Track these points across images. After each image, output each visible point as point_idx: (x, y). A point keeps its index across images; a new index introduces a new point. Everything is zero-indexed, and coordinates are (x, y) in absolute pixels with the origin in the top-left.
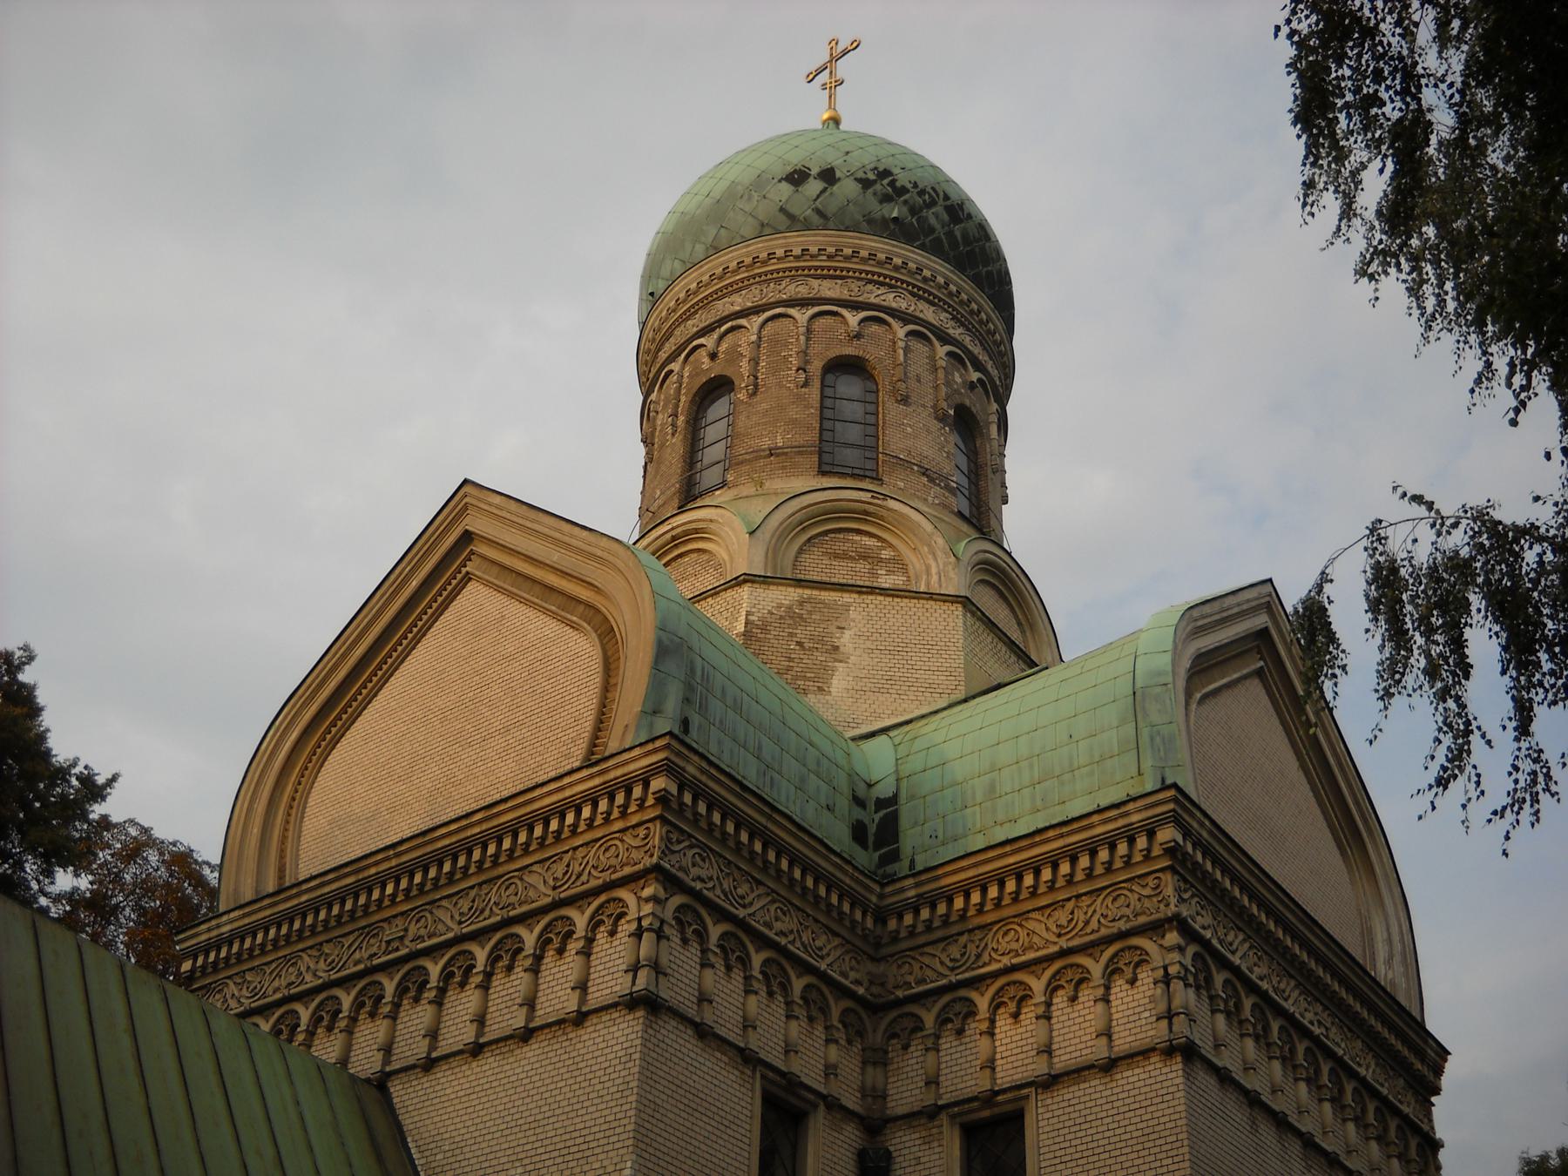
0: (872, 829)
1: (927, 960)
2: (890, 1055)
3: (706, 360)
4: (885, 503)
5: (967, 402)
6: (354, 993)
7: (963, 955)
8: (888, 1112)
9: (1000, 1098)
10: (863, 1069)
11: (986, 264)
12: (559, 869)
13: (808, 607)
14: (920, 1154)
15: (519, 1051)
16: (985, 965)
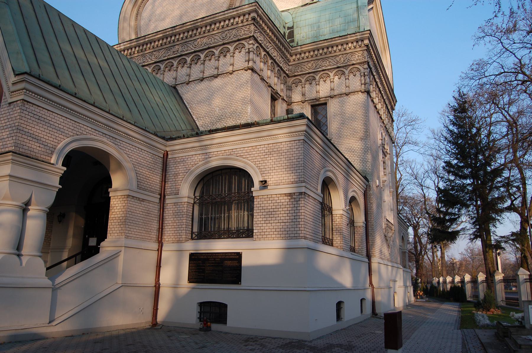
1: (302, 66)
7: (312, 66)
12: (224, 35)
16: (318, 68)
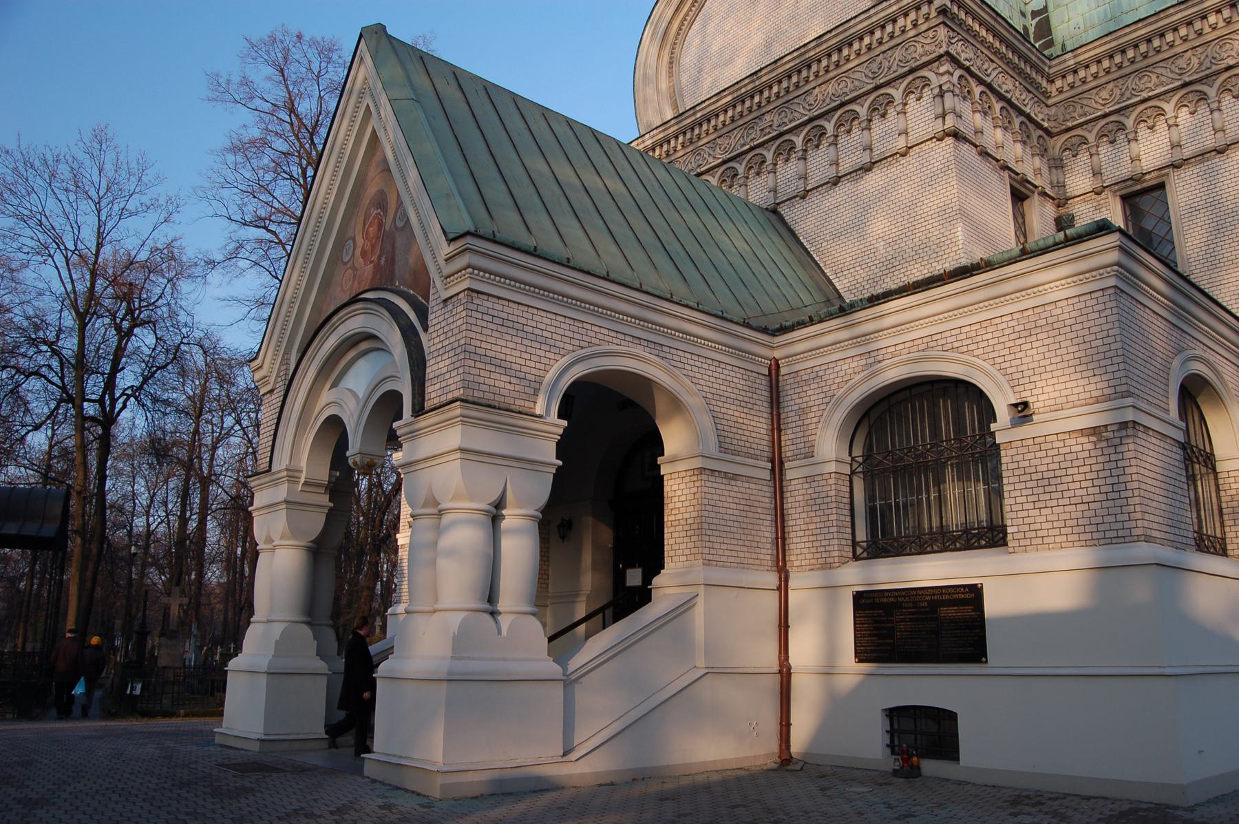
0: (1032, 30)
1: (1085, 102)
2: (1065, 162)
6: (744, 164)
7: (1111, 96)
8: (1068, 195)
9: (1147, 177)
10: (1049, 171)
12: (874, 67)
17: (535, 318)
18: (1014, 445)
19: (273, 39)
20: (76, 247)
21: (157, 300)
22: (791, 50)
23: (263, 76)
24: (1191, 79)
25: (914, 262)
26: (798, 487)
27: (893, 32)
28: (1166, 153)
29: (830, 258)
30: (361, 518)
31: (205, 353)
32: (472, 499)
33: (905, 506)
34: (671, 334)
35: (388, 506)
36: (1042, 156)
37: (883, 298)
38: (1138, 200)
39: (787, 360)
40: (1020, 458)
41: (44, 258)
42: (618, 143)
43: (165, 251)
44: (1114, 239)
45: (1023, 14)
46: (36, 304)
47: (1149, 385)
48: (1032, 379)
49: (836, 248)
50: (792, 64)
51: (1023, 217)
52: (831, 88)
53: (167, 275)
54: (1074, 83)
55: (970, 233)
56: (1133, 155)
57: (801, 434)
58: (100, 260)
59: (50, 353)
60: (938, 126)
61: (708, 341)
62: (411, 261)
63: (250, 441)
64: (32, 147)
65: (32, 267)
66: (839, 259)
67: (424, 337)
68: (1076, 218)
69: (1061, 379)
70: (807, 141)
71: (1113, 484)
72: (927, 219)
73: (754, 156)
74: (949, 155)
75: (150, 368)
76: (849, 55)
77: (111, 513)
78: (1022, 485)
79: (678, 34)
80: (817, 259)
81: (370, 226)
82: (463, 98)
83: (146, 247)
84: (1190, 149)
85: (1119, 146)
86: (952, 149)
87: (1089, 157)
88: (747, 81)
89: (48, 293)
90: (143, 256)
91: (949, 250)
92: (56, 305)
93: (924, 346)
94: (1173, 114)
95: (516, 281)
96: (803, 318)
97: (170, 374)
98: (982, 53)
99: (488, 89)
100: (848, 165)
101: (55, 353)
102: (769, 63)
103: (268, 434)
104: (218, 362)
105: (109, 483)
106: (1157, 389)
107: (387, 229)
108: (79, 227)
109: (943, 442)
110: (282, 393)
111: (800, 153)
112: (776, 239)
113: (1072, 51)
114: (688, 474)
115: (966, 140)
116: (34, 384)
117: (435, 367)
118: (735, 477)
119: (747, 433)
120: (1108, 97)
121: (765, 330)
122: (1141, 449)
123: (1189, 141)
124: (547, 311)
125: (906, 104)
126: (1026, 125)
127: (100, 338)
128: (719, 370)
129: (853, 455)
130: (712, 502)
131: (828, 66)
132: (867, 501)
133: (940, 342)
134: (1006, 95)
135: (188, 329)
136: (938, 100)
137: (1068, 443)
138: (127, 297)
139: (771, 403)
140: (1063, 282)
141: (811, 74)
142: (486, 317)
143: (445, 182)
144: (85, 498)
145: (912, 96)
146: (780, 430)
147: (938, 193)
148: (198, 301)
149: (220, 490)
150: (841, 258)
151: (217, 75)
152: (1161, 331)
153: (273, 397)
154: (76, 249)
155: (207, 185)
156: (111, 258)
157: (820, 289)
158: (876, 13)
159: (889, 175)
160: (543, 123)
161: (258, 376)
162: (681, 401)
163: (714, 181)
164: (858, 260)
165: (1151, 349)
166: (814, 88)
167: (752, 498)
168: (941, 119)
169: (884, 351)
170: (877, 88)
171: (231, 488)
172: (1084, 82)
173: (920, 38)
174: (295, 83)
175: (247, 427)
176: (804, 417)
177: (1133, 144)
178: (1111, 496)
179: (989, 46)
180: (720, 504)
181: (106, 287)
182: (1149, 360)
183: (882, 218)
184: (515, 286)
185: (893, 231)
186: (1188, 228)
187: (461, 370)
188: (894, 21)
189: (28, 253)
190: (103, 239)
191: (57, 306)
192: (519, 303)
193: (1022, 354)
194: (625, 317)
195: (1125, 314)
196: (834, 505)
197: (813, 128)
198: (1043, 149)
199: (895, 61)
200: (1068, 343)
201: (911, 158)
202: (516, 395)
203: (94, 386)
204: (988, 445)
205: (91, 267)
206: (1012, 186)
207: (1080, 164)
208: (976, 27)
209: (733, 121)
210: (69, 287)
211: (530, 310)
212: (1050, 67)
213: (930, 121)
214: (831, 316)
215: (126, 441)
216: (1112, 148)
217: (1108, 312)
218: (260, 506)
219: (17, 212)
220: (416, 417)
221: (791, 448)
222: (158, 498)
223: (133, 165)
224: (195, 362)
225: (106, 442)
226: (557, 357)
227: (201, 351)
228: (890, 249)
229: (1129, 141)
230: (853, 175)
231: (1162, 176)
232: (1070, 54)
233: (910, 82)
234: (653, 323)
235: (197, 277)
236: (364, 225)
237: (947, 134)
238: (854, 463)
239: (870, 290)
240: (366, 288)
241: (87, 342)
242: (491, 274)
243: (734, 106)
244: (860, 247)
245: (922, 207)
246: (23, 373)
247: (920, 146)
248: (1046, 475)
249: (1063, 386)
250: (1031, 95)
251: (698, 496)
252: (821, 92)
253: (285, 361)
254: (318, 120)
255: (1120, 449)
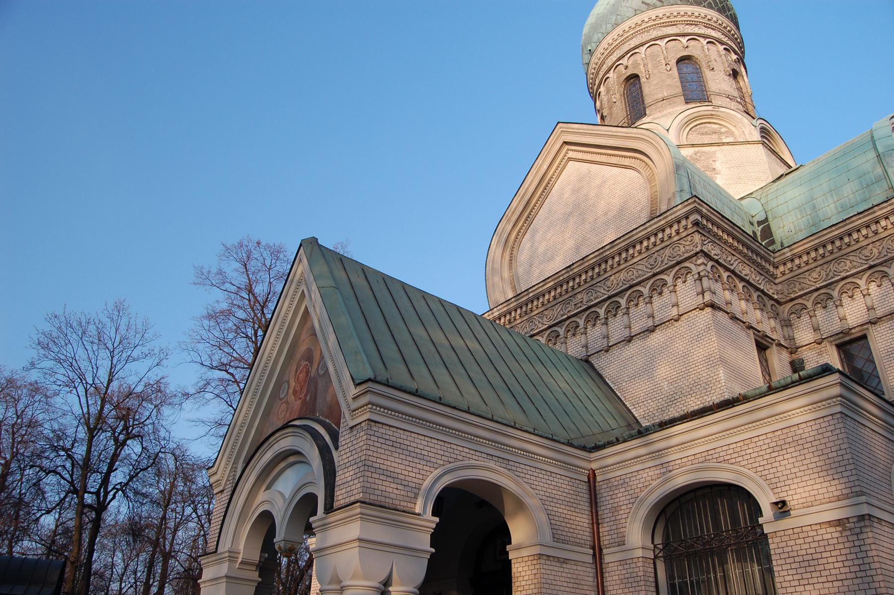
0: (759, 234)
1: (802, 280)
2: (792, 322)
3: (623, 69)
4: (719, 110)
5: (735, 68)
7: (819, 276)
9: (853, 331)
10: (782, 329)
11: (729, 11)
12: (652, 261)
13: (698, 154)
14: (818, 360)
15: (652, 336)
17: (416, 440)
18: (778, 534)
19: (241, 245)
20: (93, 382)
21: (146, 420)
22: (593, 251)
23: (233, 269)
24: (875, 263)
25: (690, 396)
26: (614, 569)
27: (663, 238)
28: (865, 314)
29: (629, 394)
30: (281, 588)
31: (176, 459)
32: (366, 578)
33: (698, 582)
34: (515, 452)
35: (301, 578)
36: (776, 318)
37: (670, 424)
38: (848, 347)
39: (601, 470)
40: (784, 544)
41: (71, 389)
42: (475, 315)
43: (155, 386)
44: (835, 377)
45: (752, 224)
46: (60, 420)
47: (876, 486)
48: (787, 483)
49: (632, 386)
50: (594, 260)
51: (767, 361)
52: (622, 276)
53: (154, 403)
54: (792, 268)
55: (729, 375)
56: (841, 316)
57: (615, 527)
58: (109, 391)
59: (65, 457)
60: (700, 300)
61: (542, 457)
62: (329, 398)
63: (202, 526)
64: (72, 313)
65: (61, 395)
66: (635, 394)
67: (335, 454)
68: (805, 362)
69: (809, 483)
70: (607, 312)
71: (859, 565)
72: (697, 365)
73: (571, 323)
74: (709, 320)
75: (135, 470)
76: (633, 254)
77: (94, 579)
78: (788, 566)
79: (515, 241)
80: (619, 395)
81: (300, 373)
82: (368, 285)
83: (142, 383)
84: (881, 310)
85: (829, 310)
86: (711, 316)
87: (809, 318)
88: (564, 272)
89: (70, 414)
90: (139, 389)
91: (715, 387)
92: (75, 422)
93: (703, 459)
94: (866, 287)
95: (403, 414)
96: (612, 439)
97: (150, 473)
98: (726, 250)
99: (386, 279)
100: (637, 328)
101: (69, 457)
102: (578, 259)
103: (217, 524)
104: (184, 466)
105: (95, 555)
106: (883, 489)
107: (312, 375)
108: (97, 368)
109: (723, 532)
110: (230, 493)
111: (603, 320)
112: (590, 381)
113: (788, 247)
114: (530, 558)
115: (720, 309)
116: (52, 479)
117: (342, 477)
118: (566, 561)
119: (574, 527)
120: (817, 277)
121: (583, 448)
122: (877, 536)
123: (879, 305)
124: (425, 436)
125: (676, 286)
126: (762, 297)
127: (102, 447)
128: (551, 479)
129: (655, 543)
130: (549, 581)
131: (619, 261)
132: (668, 580)
133: (714, 456)
134: (745, 277)
135: (166, 442)
136: (698, 282)
137: (820, 532)
138: (125, 418)
139: (591, 503)
140: (802, 410)
141: (608, 267)
142: (380, 440)
143: (354, 343)
144: (76, 567)
145: (680, 280)
146: (598, 524)
147: (703, 346)
148: (175, 421)
149: (177, 563)
150: (637, 394)
151: (202, 268)
152: (880, 444)
153: (223, 496)
154: (93, 383)
155: (188, 340)
156: (117, 390)
157: (623, 417)
158: (650, 226)
159: (668, 335)
160: (423, 303)
161: (212, 480)
162: (523, 502)
163: (543, 340)
164: (649, 395)
165: (875, 458)
166: (611, 276)
167: (580, 577)
168: (701, 295)
169: (673, 463)
170: (654, 275)
171: (185, 561)
172: (799, 267)
173: (681, 242)
174: (253, 273)
175: (201, 515)
176: (616, 514)
177: (840, 309)
178: (859, 574)
179: (730, 246)
180: (555, 583)
181: (111, 410)
182: (874, 466)
183: (665, 365)
184: (402, 418)
185: (674, 374)
186: (888, 366)
187: (361, 479)
188: (663, 231)
189: (60, 385)
190: (113, 376)
191: (75, 423)
192: (404, 430)
193: (777, 464)
194: (478, 439)
195: (851, 433)
196: (642, 583)
197: (611, 303)
198: (775, 313)
199: (666, 257)
200: (811, 455)
201: (682, 322)
202: (401, 498)
203: (94, 482)
204: (758, 535)
205: (102, 395)
206: (756, 340)
207: (803, 323)
208: (720, 233)
209: (555, 298)
210: (85, 410)
211: (413, 435)
212: (774, 258)
213: (694, 297)
214: (632, 438)
215: (112, 523)
216: (825, 312)
217: (838, 431)
218: (206, 580)
219: (57, 357)
220: (327, 514)
221: (608, 538)
222: (131, 568)
223: (139, 326)
224: (168, 466)
225: (97, 523)
226: (432, 469)
227: (173, 458)
228: (672, 386)
229: (837, 307)
230: (641, 335)
231: (864, 330)
232: (787, 249)
233: (677, 271)
234: (501, 444)
235: (176, 404)
236: (296, 374)
237: (707, 305)
238: (656, 549)
239: (659, 417)
240: (295, 417)
241: (93, 450)
242: (385, 409)
243: (555, 289)
244: (650, 386)
245: (693, 357)
246: (44, 471)
247: (688, 314)
248: (806, 558)
249: (810, 488)
250: (763, 277)
251: (538, 576)
252: (615, 278)
253: (234, 469)
254: (267, 298)
255: (861, 537)
